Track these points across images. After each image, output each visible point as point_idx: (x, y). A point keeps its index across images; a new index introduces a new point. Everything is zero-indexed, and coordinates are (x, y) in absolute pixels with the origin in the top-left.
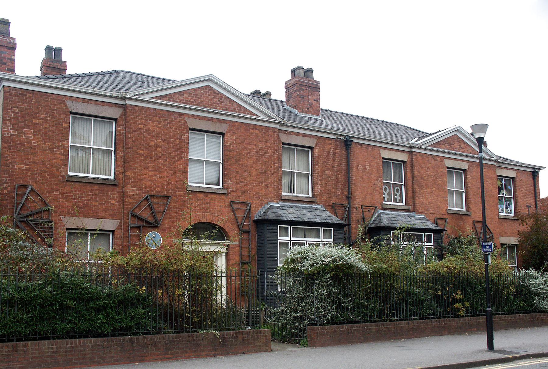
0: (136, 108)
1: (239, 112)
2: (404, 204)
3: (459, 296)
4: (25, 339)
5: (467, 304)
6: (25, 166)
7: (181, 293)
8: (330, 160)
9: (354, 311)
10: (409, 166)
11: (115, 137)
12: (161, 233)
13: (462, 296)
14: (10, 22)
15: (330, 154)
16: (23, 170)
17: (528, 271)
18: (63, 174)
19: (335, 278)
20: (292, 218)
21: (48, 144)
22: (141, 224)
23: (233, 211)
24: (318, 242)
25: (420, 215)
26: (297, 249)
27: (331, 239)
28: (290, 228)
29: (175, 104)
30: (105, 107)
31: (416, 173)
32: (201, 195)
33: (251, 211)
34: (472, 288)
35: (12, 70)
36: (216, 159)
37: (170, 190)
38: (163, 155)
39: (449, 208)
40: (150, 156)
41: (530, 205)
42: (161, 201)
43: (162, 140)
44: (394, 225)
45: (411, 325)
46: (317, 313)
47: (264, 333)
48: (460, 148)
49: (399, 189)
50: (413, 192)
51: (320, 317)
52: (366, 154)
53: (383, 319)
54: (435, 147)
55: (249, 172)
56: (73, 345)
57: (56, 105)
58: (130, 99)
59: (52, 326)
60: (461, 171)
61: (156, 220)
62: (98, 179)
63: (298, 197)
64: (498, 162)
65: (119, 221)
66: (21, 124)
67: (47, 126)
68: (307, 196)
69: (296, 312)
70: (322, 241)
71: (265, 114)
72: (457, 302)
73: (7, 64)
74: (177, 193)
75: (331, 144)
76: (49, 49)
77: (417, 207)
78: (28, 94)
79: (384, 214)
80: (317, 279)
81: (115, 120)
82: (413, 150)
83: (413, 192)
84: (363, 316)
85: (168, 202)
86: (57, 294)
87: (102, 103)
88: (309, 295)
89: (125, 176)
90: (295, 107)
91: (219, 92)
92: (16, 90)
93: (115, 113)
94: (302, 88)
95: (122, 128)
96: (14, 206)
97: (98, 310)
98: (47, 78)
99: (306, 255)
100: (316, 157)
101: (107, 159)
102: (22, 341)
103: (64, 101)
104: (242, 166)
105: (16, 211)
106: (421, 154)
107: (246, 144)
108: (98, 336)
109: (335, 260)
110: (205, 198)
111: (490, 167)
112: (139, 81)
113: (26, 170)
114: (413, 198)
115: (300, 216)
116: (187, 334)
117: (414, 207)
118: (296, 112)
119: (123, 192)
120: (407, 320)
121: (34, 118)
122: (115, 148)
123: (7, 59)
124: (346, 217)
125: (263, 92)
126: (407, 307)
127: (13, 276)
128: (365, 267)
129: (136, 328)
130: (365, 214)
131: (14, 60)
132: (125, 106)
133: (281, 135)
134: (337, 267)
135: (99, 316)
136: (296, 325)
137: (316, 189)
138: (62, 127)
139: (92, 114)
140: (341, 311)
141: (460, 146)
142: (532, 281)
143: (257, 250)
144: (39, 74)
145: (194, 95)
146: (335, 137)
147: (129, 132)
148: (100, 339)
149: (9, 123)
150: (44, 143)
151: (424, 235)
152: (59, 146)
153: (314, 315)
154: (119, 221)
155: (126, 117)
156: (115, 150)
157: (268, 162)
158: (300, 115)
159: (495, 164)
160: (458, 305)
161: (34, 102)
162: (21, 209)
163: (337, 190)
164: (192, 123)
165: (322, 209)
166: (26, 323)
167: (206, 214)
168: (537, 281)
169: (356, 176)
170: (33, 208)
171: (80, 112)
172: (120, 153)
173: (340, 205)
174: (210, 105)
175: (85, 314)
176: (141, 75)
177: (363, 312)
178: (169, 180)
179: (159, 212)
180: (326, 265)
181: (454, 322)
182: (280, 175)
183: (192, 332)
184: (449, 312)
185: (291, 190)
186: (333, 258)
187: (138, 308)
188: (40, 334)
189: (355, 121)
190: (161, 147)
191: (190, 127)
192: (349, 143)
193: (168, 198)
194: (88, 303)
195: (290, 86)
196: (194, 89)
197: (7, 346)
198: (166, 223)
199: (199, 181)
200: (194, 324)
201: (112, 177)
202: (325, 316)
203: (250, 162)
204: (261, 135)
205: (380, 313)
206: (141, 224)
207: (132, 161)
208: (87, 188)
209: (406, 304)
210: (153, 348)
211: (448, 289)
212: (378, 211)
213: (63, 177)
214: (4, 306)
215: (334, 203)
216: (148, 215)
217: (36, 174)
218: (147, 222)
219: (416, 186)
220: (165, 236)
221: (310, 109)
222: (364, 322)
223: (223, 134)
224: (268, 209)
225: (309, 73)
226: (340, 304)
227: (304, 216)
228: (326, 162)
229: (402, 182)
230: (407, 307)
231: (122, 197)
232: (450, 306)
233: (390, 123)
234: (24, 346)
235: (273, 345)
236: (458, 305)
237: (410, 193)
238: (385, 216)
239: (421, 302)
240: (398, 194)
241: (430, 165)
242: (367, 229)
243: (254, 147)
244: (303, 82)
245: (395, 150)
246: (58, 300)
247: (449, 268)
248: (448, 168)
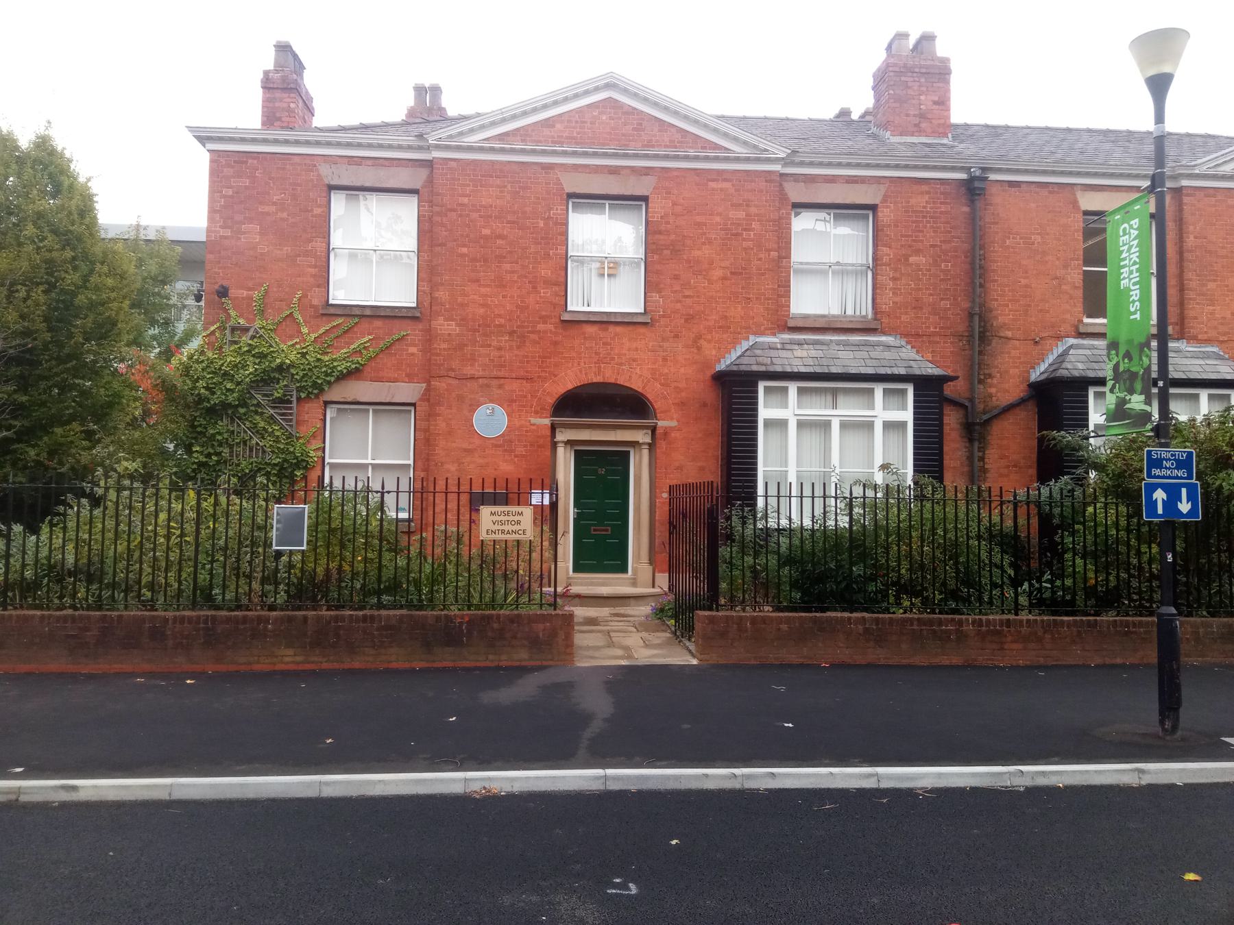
0: (453, 164)
8: (922, 231)
12: (505, 406)
15: (924, 217)
21: (287, 249)
25: (1199, 347)
32: (590, 330)
37: (524, 322)
38: (510, 252)
43: (508, 222)
52: (1033, 205)
55: (704, 273)
65: (424, 385)
66: (239, 217)
67: (285, 215)
71: (745, 143)
74: (541, 327)
78: (250, 161)
82: (1183, 184)
87: (386, 163)
91: (635, 109)
92: (228, 156)
100: (884, 226)
103: (315, 166)
106: (1211, 191)
107: (698, 214)
110: (602, 334)
119: (428, 331)
121: (261, 203)
138: (312, 216)
139: (367, 184)
144: (259, 127)
145: (577, 122)
152: (307, 251)
154: (424, 385)
157: (752, 249)
161: (261, 173)
164: (572, 184)
167: (602, 365)
178: (522, 301)
191: (569, 189)
192: (977, 184)
196: (580, 111)
203: (705, 252)
204: (736, 190)
220: (513, 411)
228: (911, 236)
243: (718, 219)
245: (1124, 189)
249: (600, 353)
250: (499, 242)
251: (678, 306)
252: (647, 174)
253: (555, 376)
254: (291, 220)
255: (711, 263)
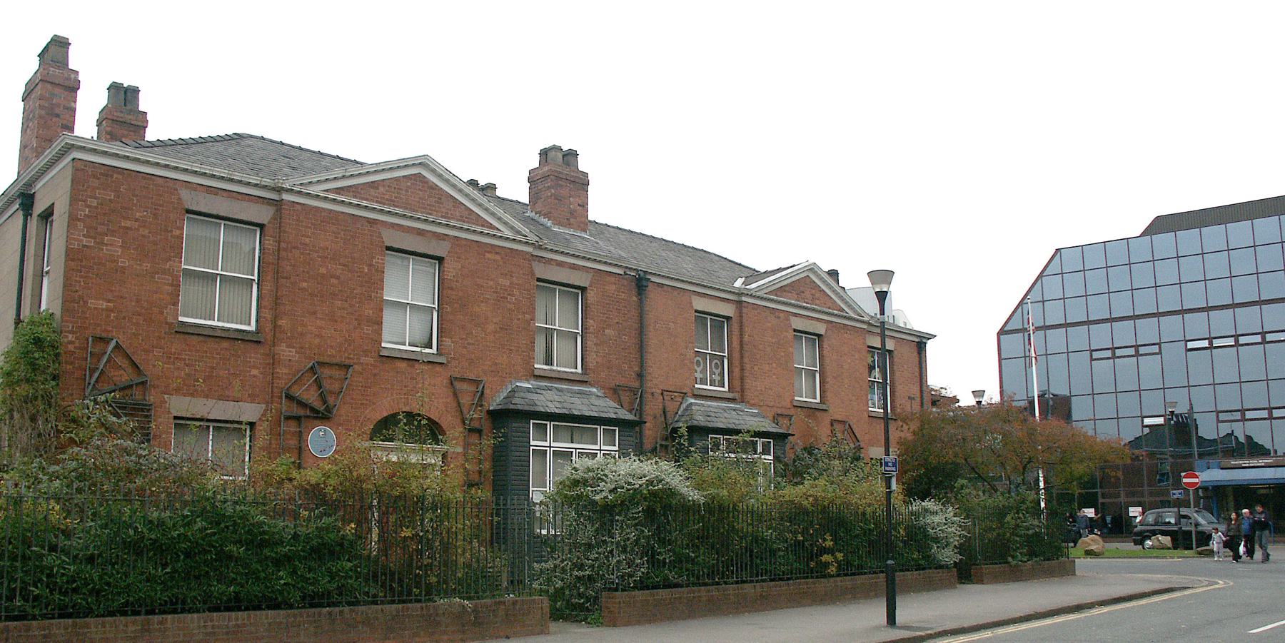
0: (299, 207)
1: (468, 222)
2: (726, 389)
3: (829, 543)
4: (160, 610)
5: (840, 556)
6: (105, 304)
7: (410, 535)
9: (675, 567)
10: (735, 326)
11: (259, 257)
13: (832, 543)
14: (70, 42)
16: (103, 310)
17: (923, 504)
18: (170, 319)
19: (650, 513)
20: (552, 408)
22: (301, 412)
23: (455, 395)
24: (544, 448)
26: (589, 462)
27: (546, 441)
28: (550, 426)
29: (364, 203)
30: (245, 204)
31: (746, 338)
32: (403, 365)
33: (485, 395)
34: (846, 529)
35: (72, 131)
36: (427, 303)
39: (796, 398)
40: (318, 292)
41: (913, 396)
42: (337, 373)
43: (340, 264)
44: (739, 427)
45: (759, 590)
46: (618, 570)
47: (539, 604)
48: (814, 298)
49: (701, 362)
50: (742, 370)
51: (622, 576)
53: (717, 580)
54: (776, 295)
56: (239, 622)
57: (161, 196)
58: (290, 191)
59: (204, 588)
60: (576, 291)
61: (327, 406)
62: (229, 330)
63: (559, 371)
64: (869, 324)
65: (264, 406)
66: (101, 229)
68: (573, 370)
69: (581, 567)
70: (550, 447)
71: (512, 228)
72: (825, 553)
73: (61, 116)
74: (363, 359)
75: (615, 284)
76: (115, 89)
77: (747, 395)
78: (115, 176)
79: (696, 404)
80: (619, 514)
81: (261, 226)
83: (742, 370)
84: (688, 576)
85: (349, 376)
86: (214, 534)
87: (240, 197)
88: (605, 540)
89: (275, 326)
90: (548, 216)
91: (437, 186)
93: (263, 214)
94: (560, 182)
95: (273, 241)
96: (85, 375)
97: (278, 563)
98: (138, 145)
99: (602, 473)
101: (209, 290)
102: (155, 614)
104: (471, 316)
105: (89, 384)
107: (478, 277)
108: (277, 607)
109: (651, 482)
111: (857, 332)
112: (284, 157)
113: (109, 310)
114: (742, 379)
115: (565, 405)
116: (418, 605)
117: (742, 396)
118: (549, 224)
120: (752, 581)
121: (124, 218)
122: (259, 275)
123: (62, 108)
124: (637, 410)
125: (482, 182)
126: (751, 561)
127: (140, 501)
128: (693, 495)
129: (336, 594)
130: (668, 404)
131: (75, 110)
132: (279, 203)
133: (535, 265)
134: (654, 494)
135: (281, 573)
136: (582, 590)
137: (589, 359)
139: (222, 214)
140: (653, 566)
141: (814, 295)
142: (930, 519)
143: (493, 462)
146: (621, 272)
147: (285, 250)
148: (282, 612)
149: (80, 225)
150: (139, 263)
151: (760, 442)
153: (613, 574)
154: (264, 406)
155: (280, 223)
156: (258, 280)
158: (556, 229)
159: (865, 326)
160: (826, 558)
162: (97, 381)
163: (623, 363)
164: (391, 239)
165: (599, 394)
166: (162, 583)
168: (937, 519)
169: (653, 339)
170: (119, 379)
171: (203, 210)
172: (267, 286)
173: (626, 389)
174: (421, 208)
175: (257, 569)
176: (282, 143)
177: (687, 570)
179: (331, 392)
180: (635, 490)
181: (823, 585)
182: (532, 334)
183: (425, 602)
184: (812, 569)
185: (549, 361)
186: (647, 478)
187: (340, 560)
188: (184, 602)
189: (642, 244)
190: (338, 278)
192: (644, 283)
193: (347, 367)
194: (261, 550)
195: (538, 178)
197: (134, 623)
198: (343, 411)
199: (400, 340)
200: (429, 586)
201: (252, 328)
202: (630, 576)
205: (713, 572)
206: (301, 412)
207: (289, 301)
208: (211, 344)
209: (751, 556)
210: (365, 629)
211: (811, 532)
212: (687, 401)
213: (170, 325)
214: (125, 554)
215: (617, 384)
216: (314, 398)
217: (124, 318)
218: (313, 409)
219: (746, 360)
221: (572, 220)
222: (688, 586)
223: (440, 260)
224: (513, 391)
225: (570, 158)
226: (653, 556)
227: (571, 406)
229: (724, 353)
230: (751, 561)
231: (269, 364)
232: (815, 559)
233: (693, 248)
234: (161, 623)
235: (553, 626)
236: (826, 558)
237: (737, 371)
238: (698, 408)
239: (773, 553)
240: (717, 372)
241: (769, 325)
242: (669, 431)
244: (560, 173)
246: (214, 544)
247: (816, 499)
248: (795, 330)
249: (408, 386)
250: (334, 281)
251: (464, 351)
252: (444, 240)
253: (374, 404)
254: (151, 239)
255: (487, 318)
